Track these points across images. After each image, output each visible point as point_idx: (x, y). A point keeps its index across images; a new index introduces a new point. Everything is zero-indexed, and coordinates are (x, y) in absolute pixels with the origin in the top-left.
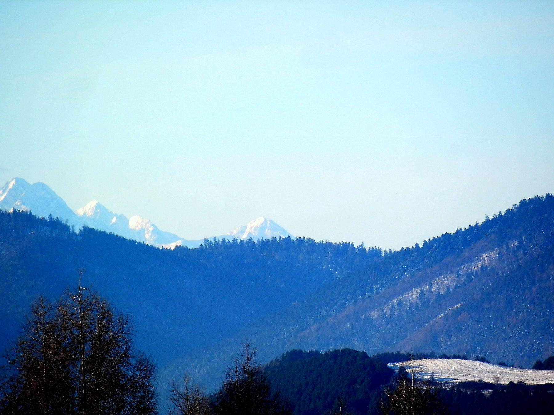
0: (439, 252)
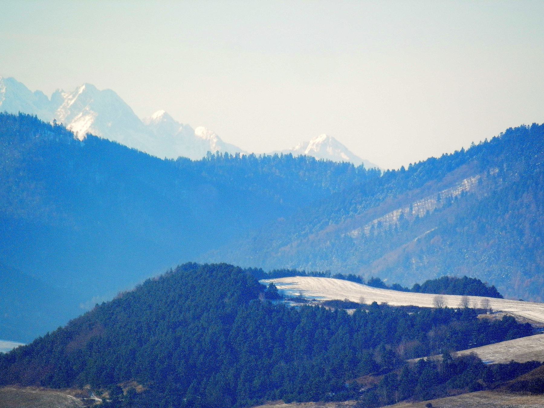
0: (423, 176)
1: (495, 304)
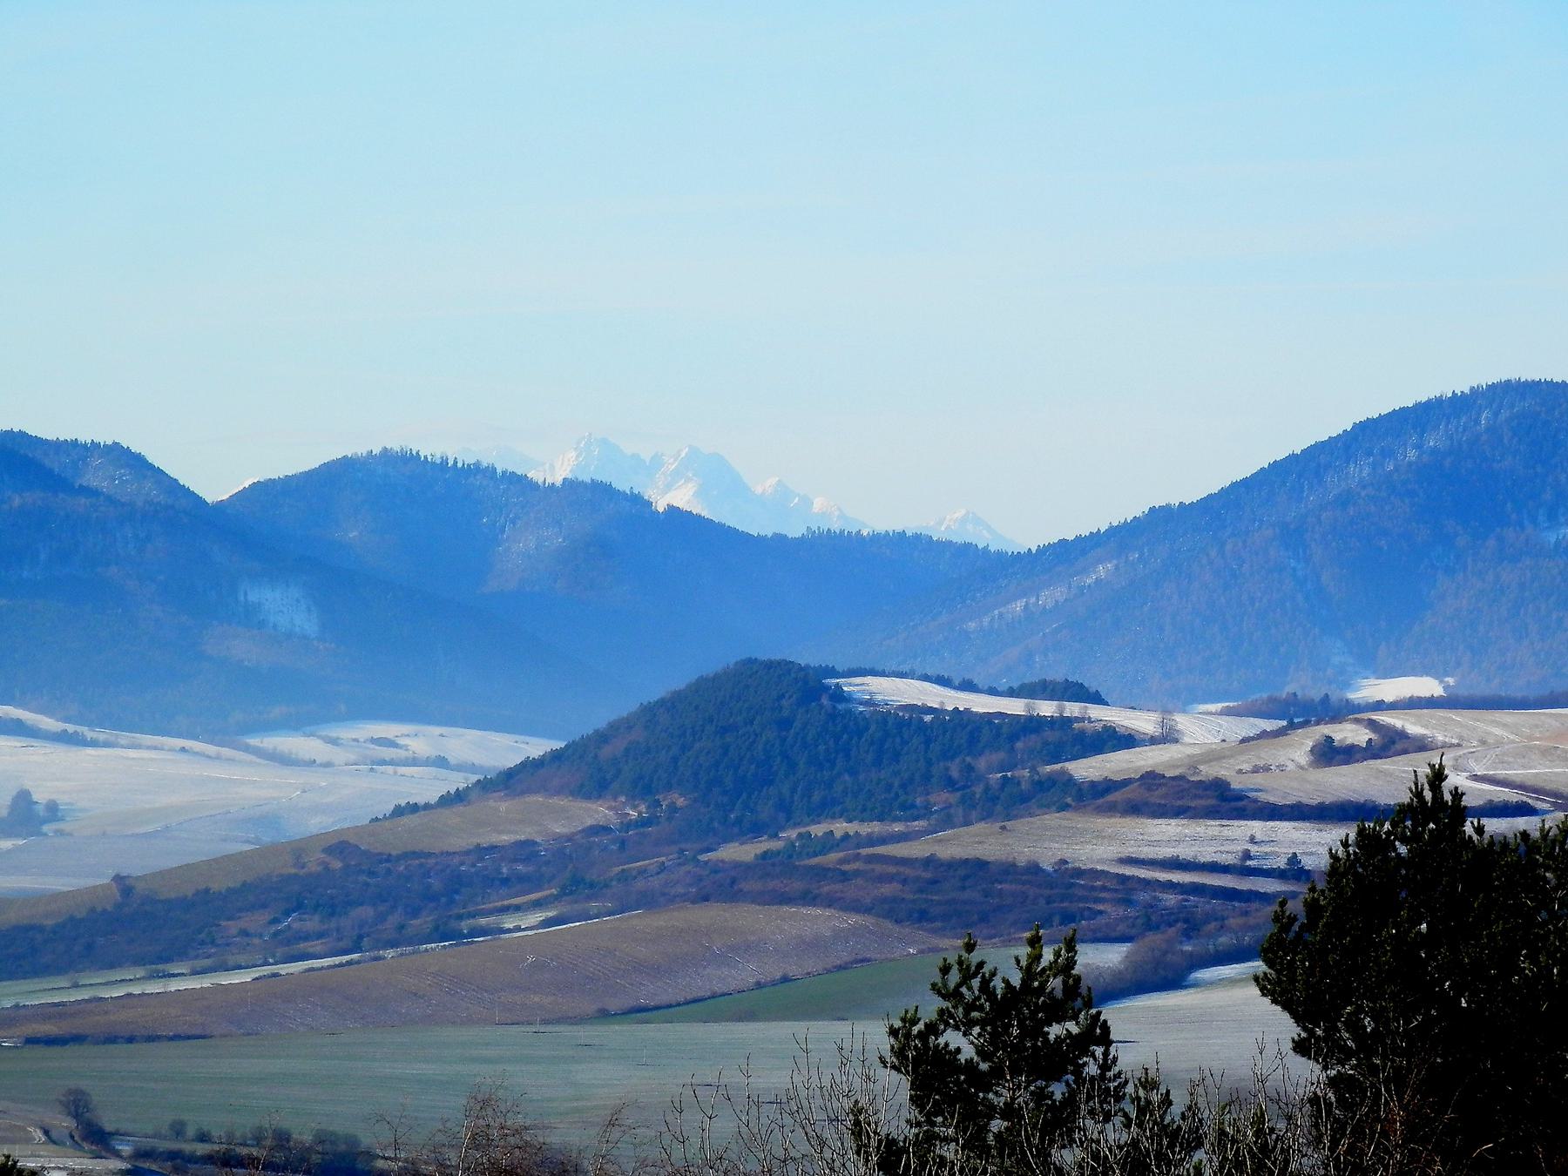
1: (1095, 712)
